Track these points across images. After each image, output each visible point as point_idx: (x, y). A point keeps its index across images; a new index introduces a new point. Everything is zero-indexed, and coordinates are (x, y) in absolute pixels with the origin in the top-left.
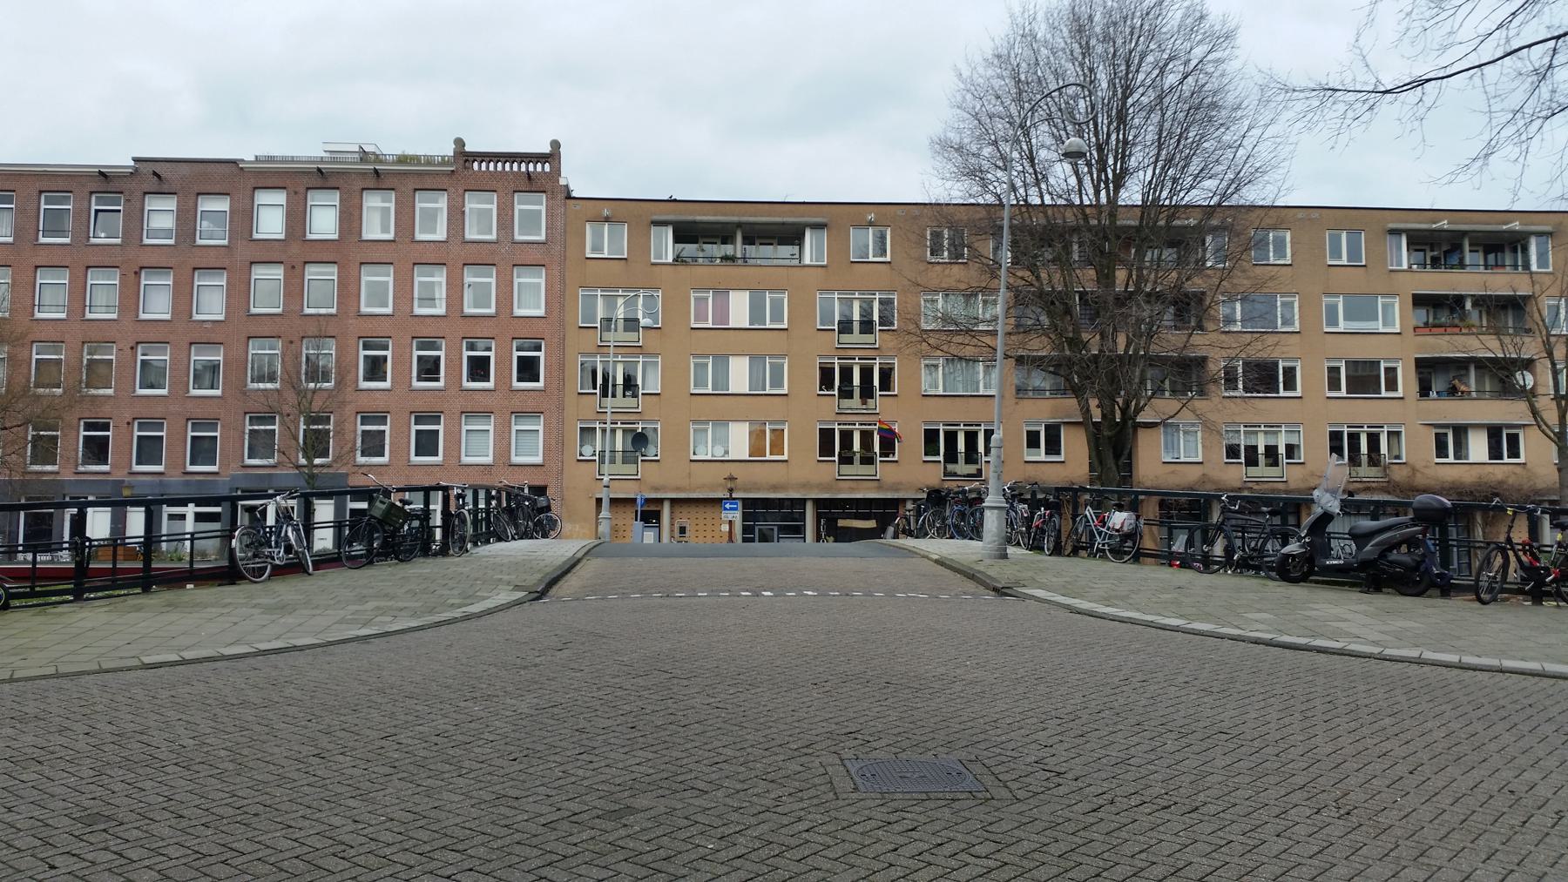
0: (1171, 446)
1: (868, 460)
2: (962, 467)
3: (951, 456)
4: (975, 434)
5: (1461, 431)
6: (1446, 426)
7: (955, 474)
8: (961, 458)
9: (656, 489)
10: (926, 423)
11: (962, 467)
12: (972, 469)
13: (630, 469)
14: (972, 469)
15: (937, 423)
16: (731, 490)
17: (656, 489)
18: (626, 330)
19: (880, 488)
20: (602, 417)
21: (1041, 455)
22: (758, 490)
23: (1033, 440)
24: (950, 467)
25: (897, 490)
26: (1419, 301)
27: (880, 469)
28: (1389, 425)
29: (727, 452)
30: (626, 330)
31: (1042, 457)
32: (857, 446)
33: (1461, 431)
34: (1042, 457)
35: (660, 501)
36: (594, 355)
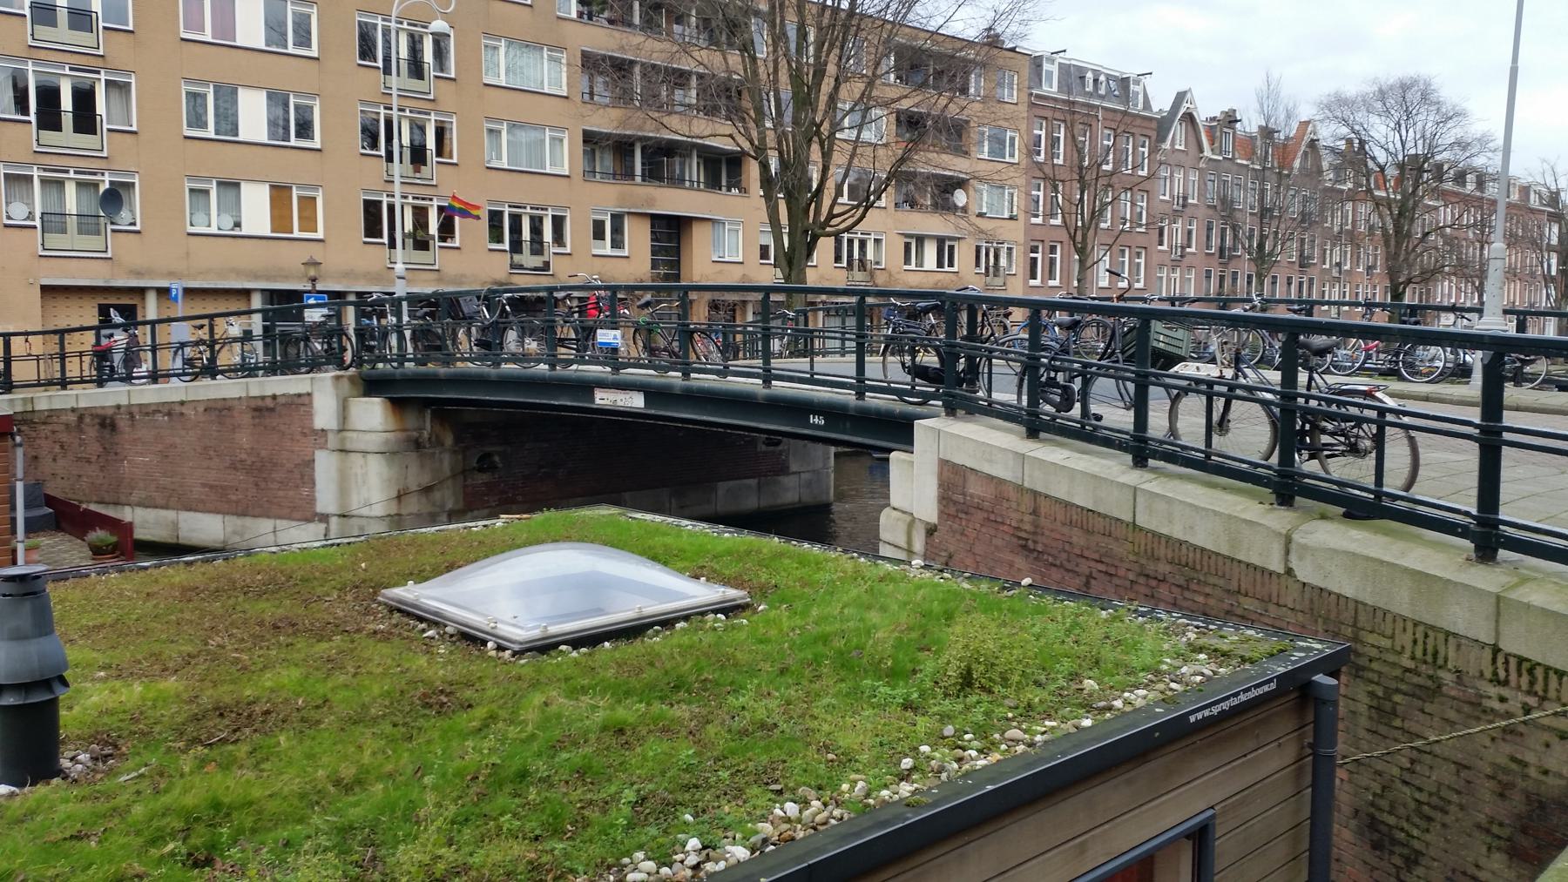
0: (717, 244)
1: (422, 245)
2: (527, 258)
3: (516, 246)
4: (541, 219)
5: (920, 240)
6: (910, 236)
7: (521, 267)
8: (526, 247)
9: (139, 274)
10: (366, 191)
11: (527, 258)
12: (537, 261)
13: (93, 242)
14: (537, 261)
15: (502, 203)
16: (314, 280)
17: (139, 274)
18: (73, 26)
19: (440, 281)
20: (389, 187)
21: (606, 248)
22: (286, 278)
23: (599, 233)
24: (517, 257)
25: (461, 283)
26: (591, 63)
27: (437, 255)
28: (554, 207)
29: (238, 225)
30: (73, 26)
31: (608, 251)
32: (526, 234)
33: (920, 240)
34: (608, 251)
35: (141, 291)
36: (377, 105)
